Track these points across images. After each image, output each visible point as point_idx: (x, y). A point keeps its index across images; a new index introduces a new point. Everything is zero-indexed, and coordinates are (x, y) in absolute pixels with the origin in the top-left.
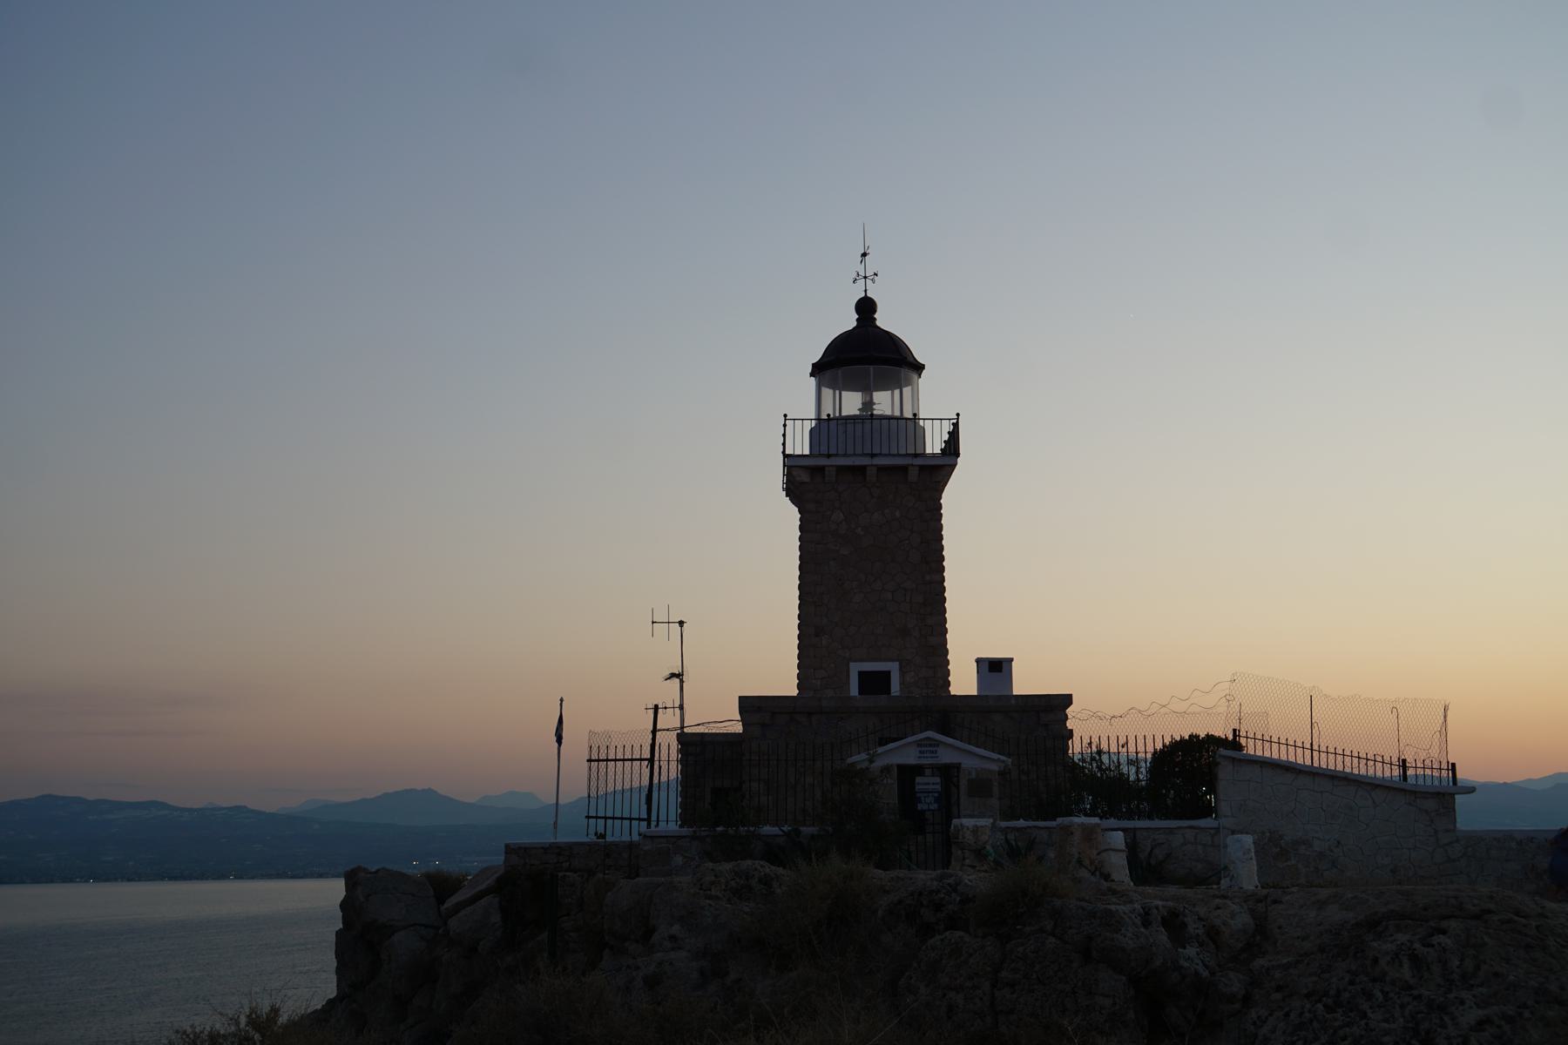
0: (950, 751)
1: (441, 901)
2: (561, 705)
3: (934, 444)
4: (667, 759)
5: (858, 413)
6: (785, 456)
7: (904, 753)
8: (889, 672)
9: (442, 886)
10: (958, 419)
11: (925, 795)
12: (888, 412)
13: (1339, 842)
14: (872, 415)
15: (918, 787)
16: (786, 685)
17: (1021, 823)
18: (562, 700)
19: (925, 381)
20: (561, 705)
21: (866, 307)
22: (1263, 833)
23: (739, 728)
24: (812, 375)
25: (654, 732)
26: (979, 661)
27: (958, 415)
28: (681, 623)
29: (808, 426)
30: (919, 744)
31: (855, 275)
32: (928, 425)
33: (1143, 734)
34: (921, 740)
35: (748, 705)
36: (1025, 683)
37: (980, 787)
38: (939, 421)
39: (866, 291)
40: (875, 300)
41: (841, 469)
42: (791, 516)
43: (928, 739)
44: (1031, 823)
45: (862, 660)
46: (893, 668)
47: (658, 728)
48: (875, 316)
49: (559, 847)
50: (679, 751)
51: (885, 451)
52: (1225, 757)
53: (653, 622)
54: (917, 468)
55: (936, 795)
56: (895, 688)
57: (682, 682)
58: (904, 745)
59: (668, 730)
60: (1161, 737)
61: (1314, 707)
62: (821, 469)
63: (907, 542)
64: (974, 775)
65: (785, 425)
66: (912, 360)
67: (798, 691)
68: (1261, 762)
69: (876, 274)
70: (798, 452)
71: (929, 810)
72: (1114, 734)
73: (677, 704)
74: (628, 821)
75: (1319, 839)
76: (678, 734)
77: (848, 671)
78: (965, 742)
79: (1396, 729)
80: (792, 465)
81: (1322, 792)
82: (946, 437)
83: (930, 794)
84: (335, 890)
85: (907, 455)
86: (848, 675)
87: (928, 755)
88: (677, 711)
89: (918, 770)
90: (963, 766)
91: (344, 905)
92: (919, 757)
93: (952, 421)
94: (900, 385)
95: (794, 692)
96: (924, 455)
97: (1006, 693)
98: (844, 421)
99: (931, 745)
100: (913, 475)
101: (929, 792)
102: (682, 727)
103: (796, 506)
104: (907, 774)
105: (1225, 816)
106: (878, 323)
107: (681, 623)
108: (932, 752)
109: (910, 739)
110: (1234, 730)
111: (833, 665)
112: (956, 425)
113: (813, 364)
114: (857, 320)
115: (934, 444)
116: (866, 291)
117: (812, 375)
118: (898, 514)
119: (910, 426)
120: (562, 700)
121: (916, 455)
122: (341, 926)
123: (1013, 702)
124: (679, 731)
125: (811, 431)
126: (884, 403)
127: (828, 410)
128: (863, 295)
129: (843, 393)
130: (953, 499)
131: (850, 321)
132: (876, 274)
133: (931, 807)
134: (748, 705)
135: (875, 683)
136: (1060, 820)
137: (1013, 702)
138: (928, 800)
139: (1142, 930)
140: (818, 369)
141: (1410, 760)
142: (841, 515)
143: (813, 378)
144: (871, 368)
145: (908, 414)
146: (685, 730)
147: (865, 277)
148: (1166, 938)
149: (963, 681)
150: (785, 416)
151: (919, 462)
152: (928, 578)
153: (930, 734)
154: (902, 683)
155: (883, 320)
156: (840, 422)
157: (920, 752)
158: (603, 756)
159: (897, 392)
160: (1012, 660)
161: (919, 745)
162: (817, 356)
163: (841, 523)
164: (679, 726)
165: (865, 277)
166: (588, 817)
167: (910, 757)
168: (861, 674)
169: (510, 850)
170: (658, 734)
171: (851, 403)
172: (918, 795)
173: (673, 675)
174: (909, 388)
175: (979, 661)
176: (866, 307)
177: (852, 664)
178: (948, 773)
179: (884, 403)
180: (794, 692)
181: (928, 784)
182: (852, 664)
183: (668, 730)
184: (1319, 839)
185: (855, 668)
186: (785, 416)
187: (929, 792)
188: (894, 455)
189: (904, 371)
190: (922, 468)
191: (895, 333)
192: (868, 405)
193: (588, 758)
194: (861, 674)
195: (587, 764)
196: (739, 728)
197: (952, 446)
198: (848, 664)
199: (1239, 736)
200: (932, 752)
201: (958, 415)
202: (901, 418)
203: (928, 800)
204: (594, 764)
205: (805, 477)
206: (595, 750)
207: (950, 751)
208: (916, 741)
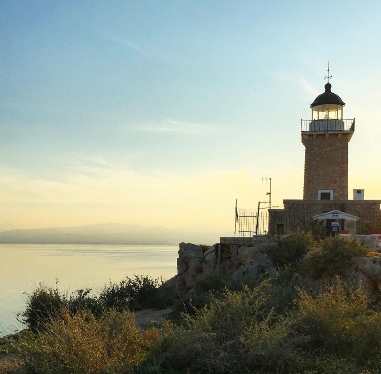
0: (342, 216)
1: (204, 251)
2: (236, 201)
3: (347, 127)
5: (324, 118)
6: (302, 132)
7: (329, 216)
8: (330, 193)
9: (204, 248)
10: (354, 119)
12: (334, 118)
14: (328, 119)
15: (332, 225)
16: (298, 194)
18: (237, 200)
19: (345, 108)
20: (236, 201)
21: (328, 86)
23: (283, 208)
24: (311, 107)
25: (259, 209)
26: (354, 190)
27: (355, 118)
28: (270, 179)
29: (308, 123)
31: (325, 77)
32: (345, 121)
35: (286, 202)
36: (367, 197)
37: (351, 225)
38: (348, 120)
39: (328, 82)
40: (331, 84)
41: (318, 135)
42: (303, 148)
44: (364, 236)
45: (322, 190)
46: (331, 192)
47: (260, 208)
48: (331, 89)
49: (235, 239)
50: (269, 214)
51: (331, 130)
53: (262, 179)
55: (338, 227)
56: (332, 198)
57: (270, 195)
59: (262, 208)
61: (236, 230)
62: (312, 135)
65: (301, 123)
66: (341, 102)
67: (303, 198)
69: (331, 76)
70: (305, 130)
73: (269, 201)
76: (268, 210)
80: (304, 133)
82: (351, 125)
84: (178, 248)
86: (330, 190)
87: (335, 216)
88: (269, 203)
89: (334, 220)
90: (346, 220)
91: (179, 252)
93: (353, 120)
95: (302, 198)
96: (344, 131)
97: (363, 199)
102: (270, 207)
103: (305, 145)
104: (329, 221)
106: (331, 91)
107: (270, 179)
109: (331, 212)
112: (354, 121)
114: (325, 90)
115: (347, 127)
116: (328, 82)
117: (311, 107)
119: (340, 122)
120: (237, 200)
121: (341, 131)
122: (179, 257)
123: (364, 202)
124: (269, 208)
125: (310, 124)
126: (332, 115)
127: (315, 117)
128: (327, 83)
130: (351, 144)
131: (323, 91)
132: (331, 76)
134: (286, 202)
135: (325, 196)
136: (372, 235)
137: (364, 202)
139: (373, 264)
140: (313, 105)
143: (311, 109)
145: (339, 118)
146: (271, 208)
147: (328, 77)
148: (380, 267)
149: (351, 197)
150: (302, 120)
151: (342, 132)
154: (334, 196)
155: (333, 90)
156: (318, 121)
158: (243, 215)
159: (336, 112)
160: (364, 190)
161: (333, 214)
163: (317, 151)
164: (269, 207)
165: (328, 77)
166: (239, 231)
168: (321, 193)
169: (222, 239)
170: (260, 209)
171: (322, 115)
172: (332, 227)
173: (268, 193)
174: (340, 110)
175: (354, 190)
176: (328, 86)
177: (319, 191)
178: (342, 221)
179: (332, 115)
180: (302, 198)
181: (335, 224)
182: (319, 191)
183: (262, 208)
185: (320, 192)
186: (302, 120)
189: (339, 106)
191: (337, 94)
194: (321, 193)
196: (283, 208)
197: (353, 128)
201: (355, 118)
202: (337, 120)
205: (307, 137)
206: (241, 213)
207: (342, 216)
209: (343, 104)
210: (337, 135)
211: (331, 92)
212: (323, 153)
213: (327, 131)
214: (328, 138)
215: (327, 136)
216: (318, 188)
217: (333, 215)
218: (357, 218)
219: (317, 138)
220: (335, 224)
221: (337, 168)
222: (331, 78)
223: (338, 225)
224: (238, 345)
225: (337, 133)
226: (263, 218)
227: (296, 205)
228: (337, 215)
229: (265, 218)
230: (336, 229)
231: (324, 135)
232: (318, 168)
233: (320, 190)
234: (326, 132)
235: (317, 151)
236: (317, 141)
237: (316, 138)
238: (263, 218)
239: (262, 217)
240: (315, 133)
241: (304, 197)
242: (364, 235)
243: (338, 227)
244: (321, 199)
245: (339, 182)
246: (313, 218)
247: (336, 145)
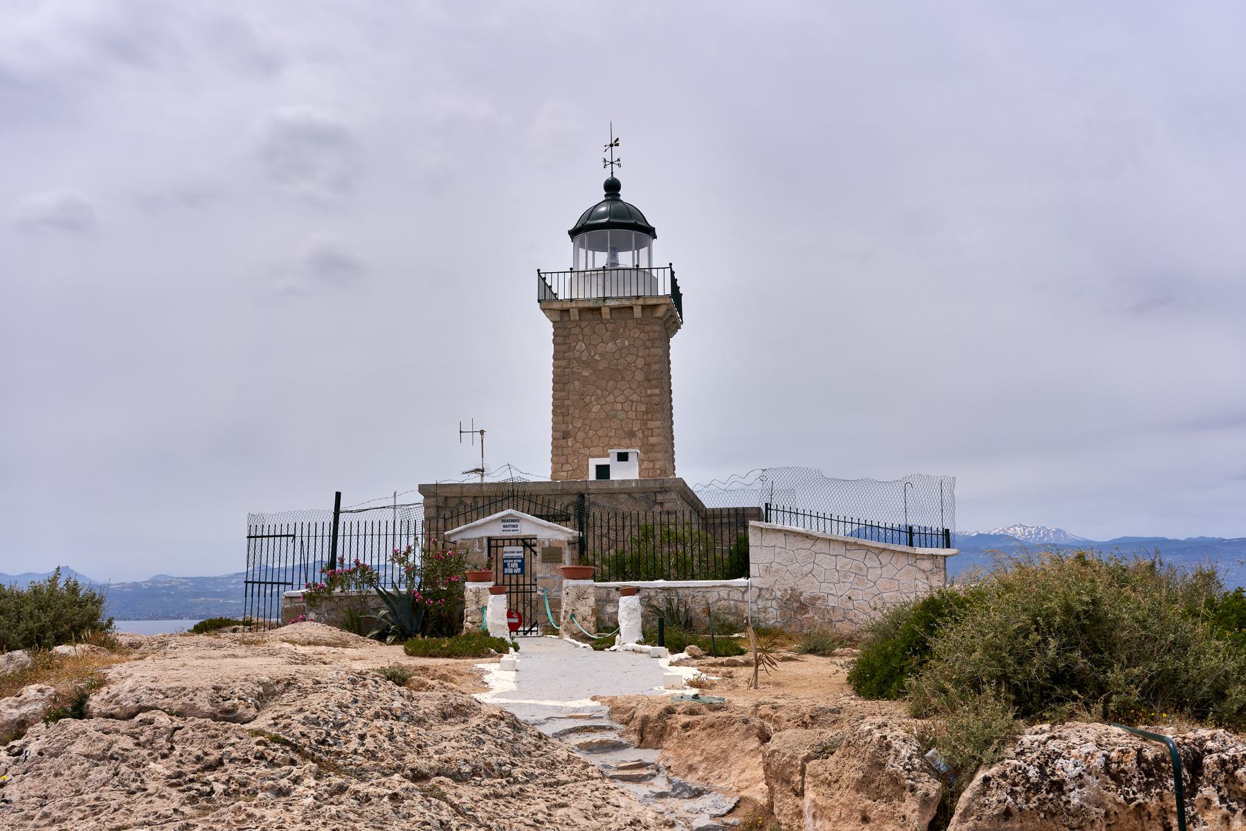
3: (664, 289)
4: (314, 535)
11: (511, 561)
13: (850, 598)
17: (661, 583)
21: (612, 187)
22: (786, 590)
27: (671, 264)
28: (482, 432)
30: (503, 519)
33: (357, 520)
34: (504, 517)
39: (612, 173)
43: (510, 515)
51: (614, 295)
52: (755, 527)
53: (461, 432)
54: (640, 307)
55: (520, 561)
58: (491, 521)
60: (356, 523)
62: (568, 311)
63: (634, 364)
64: (547, 544)
68: (784, 530)
71: (514, 573)
72: (364, 519)
74: (258, 585)
75: (833, 595)
77: (588, 465)
78: (552, 521)
79: (903, 507)
81: (836, 556)
83: (515, 561)
85: (631, 297)
92: (503, 531)
94: (639, 247)
98: (596, 272)
99: (512, 521)
100: (638, 312)
101: (513, 559)
104: (493, 544)
105: (754, 577)
107: (482, 432)
108: (514, 526)
110: (767, 504)
111: (576, 461)
113: (654, 228)
116: (612, 173)
118: (627, 343)
129: (596, 252)
133: (516, 571)
138: (513, 566)
140: (573, 233)
141: (915, 529)
142: (584, 345)
144: (634, 232)
147: (612, 163)
150: (539, 270)
151: (641, 302)
152: (649, 392)
153: (510, 511)
157: (504, 526)
159: (636, 252)
161: (503, 521)
162: (571, 227)
163: (583, 351)
165: (612, 163)
166: (247, 582)
167: (497, 531)
176: (612, 187)
178: (527, 543)
181: (513, 552)
184: (833, 595)
186: (539, 270)
187: (513, 559)
188: (621, 298)
190: (644, 307)
192: (613, 256)
193: (247, 535)
194: (598, 467)
195: (246, 540)
197: (676, 294)
198: (588, 460)
199: (770, 509)
200: (514, 526)
201: (671, 264)
203: (513, 566)
204: (253, 540)
208: (502, 517)
209: (651, 232)
210: (631, 308)
211: (621, 201)
212: (597, 357)
213: (605, 299)
214: (609, 317)
215: (605, 311)
216: (587, 452)
217: (504, 526)
218: (570, 533)
219: (580, 318)
220: (513, 552)
221: (635, 397)
222: (619, 165)
223: (522, 555)
224: (800, 814)
225: (627, 303)
226: (312, 540)
227: (457, 501)
228: (515, 523)
229: (319, 539)
230: (516, 565)
231: (599, 309)
232: (587, 399)
233: (594, 457)
234: (600, 304)
235: (583, 351)
236: (583, 326)
237: (578, 318)
238: (312, 540)
239: (360, 537)
240: (574, 305)
241: (486, 483)
242: (668, 578)
243: (523, 560)
244: (597, 478)
245: (640, 435)
246: (449, 536)
247: (630, 335)
